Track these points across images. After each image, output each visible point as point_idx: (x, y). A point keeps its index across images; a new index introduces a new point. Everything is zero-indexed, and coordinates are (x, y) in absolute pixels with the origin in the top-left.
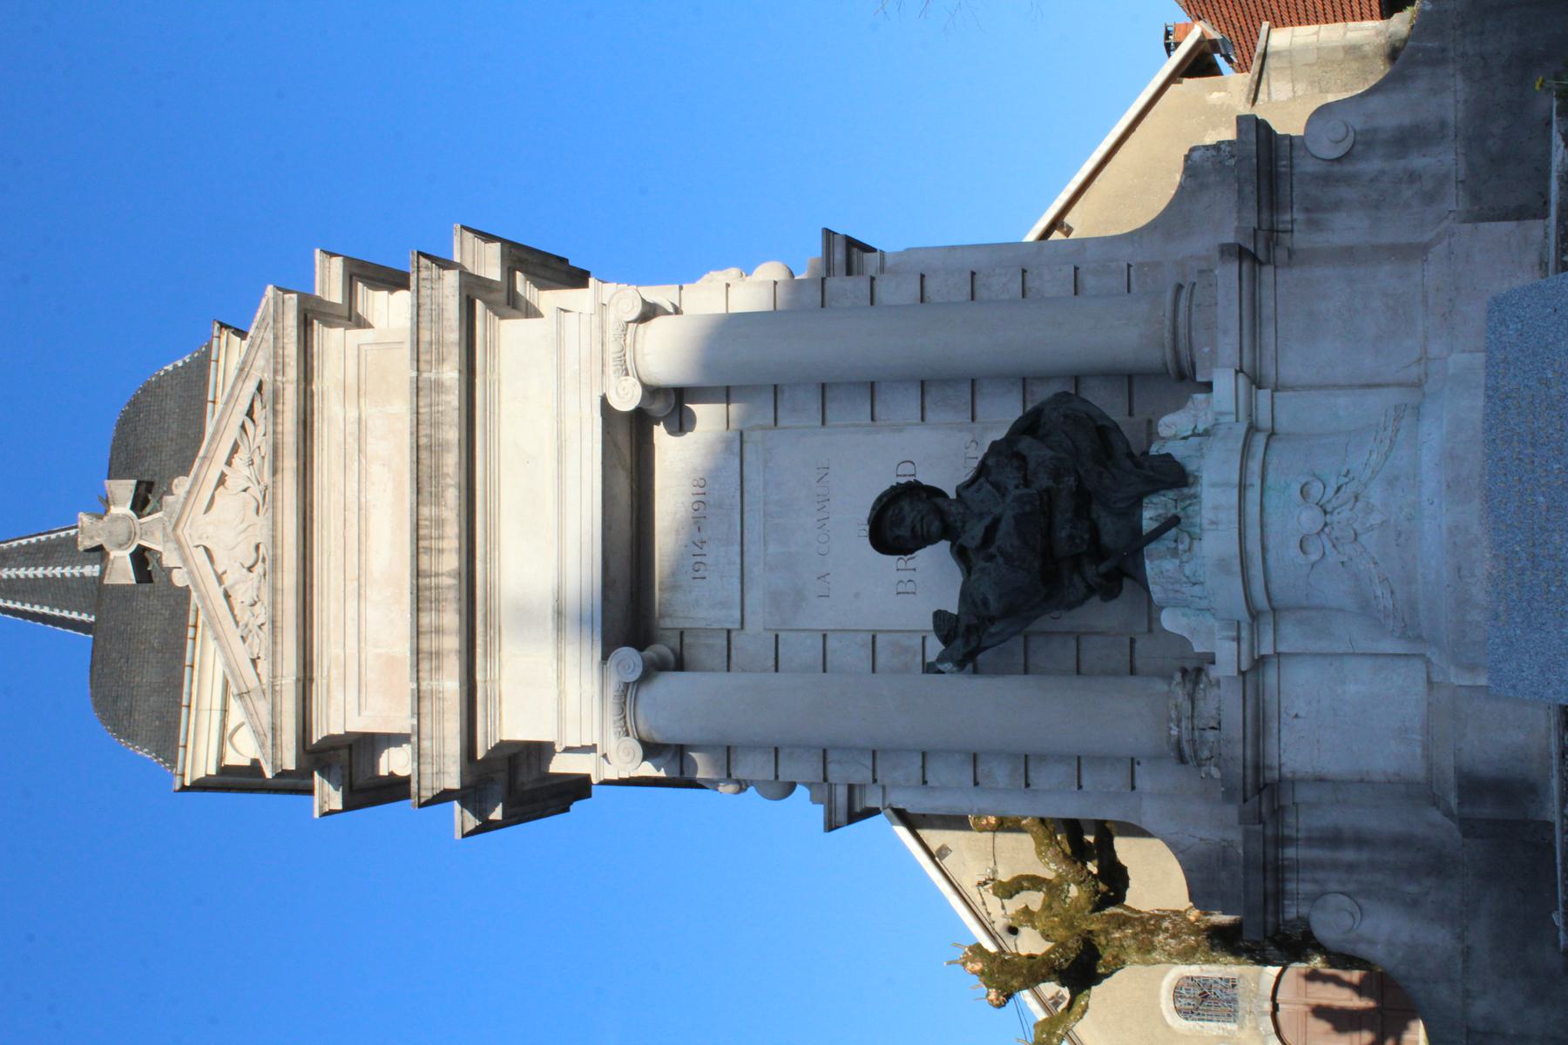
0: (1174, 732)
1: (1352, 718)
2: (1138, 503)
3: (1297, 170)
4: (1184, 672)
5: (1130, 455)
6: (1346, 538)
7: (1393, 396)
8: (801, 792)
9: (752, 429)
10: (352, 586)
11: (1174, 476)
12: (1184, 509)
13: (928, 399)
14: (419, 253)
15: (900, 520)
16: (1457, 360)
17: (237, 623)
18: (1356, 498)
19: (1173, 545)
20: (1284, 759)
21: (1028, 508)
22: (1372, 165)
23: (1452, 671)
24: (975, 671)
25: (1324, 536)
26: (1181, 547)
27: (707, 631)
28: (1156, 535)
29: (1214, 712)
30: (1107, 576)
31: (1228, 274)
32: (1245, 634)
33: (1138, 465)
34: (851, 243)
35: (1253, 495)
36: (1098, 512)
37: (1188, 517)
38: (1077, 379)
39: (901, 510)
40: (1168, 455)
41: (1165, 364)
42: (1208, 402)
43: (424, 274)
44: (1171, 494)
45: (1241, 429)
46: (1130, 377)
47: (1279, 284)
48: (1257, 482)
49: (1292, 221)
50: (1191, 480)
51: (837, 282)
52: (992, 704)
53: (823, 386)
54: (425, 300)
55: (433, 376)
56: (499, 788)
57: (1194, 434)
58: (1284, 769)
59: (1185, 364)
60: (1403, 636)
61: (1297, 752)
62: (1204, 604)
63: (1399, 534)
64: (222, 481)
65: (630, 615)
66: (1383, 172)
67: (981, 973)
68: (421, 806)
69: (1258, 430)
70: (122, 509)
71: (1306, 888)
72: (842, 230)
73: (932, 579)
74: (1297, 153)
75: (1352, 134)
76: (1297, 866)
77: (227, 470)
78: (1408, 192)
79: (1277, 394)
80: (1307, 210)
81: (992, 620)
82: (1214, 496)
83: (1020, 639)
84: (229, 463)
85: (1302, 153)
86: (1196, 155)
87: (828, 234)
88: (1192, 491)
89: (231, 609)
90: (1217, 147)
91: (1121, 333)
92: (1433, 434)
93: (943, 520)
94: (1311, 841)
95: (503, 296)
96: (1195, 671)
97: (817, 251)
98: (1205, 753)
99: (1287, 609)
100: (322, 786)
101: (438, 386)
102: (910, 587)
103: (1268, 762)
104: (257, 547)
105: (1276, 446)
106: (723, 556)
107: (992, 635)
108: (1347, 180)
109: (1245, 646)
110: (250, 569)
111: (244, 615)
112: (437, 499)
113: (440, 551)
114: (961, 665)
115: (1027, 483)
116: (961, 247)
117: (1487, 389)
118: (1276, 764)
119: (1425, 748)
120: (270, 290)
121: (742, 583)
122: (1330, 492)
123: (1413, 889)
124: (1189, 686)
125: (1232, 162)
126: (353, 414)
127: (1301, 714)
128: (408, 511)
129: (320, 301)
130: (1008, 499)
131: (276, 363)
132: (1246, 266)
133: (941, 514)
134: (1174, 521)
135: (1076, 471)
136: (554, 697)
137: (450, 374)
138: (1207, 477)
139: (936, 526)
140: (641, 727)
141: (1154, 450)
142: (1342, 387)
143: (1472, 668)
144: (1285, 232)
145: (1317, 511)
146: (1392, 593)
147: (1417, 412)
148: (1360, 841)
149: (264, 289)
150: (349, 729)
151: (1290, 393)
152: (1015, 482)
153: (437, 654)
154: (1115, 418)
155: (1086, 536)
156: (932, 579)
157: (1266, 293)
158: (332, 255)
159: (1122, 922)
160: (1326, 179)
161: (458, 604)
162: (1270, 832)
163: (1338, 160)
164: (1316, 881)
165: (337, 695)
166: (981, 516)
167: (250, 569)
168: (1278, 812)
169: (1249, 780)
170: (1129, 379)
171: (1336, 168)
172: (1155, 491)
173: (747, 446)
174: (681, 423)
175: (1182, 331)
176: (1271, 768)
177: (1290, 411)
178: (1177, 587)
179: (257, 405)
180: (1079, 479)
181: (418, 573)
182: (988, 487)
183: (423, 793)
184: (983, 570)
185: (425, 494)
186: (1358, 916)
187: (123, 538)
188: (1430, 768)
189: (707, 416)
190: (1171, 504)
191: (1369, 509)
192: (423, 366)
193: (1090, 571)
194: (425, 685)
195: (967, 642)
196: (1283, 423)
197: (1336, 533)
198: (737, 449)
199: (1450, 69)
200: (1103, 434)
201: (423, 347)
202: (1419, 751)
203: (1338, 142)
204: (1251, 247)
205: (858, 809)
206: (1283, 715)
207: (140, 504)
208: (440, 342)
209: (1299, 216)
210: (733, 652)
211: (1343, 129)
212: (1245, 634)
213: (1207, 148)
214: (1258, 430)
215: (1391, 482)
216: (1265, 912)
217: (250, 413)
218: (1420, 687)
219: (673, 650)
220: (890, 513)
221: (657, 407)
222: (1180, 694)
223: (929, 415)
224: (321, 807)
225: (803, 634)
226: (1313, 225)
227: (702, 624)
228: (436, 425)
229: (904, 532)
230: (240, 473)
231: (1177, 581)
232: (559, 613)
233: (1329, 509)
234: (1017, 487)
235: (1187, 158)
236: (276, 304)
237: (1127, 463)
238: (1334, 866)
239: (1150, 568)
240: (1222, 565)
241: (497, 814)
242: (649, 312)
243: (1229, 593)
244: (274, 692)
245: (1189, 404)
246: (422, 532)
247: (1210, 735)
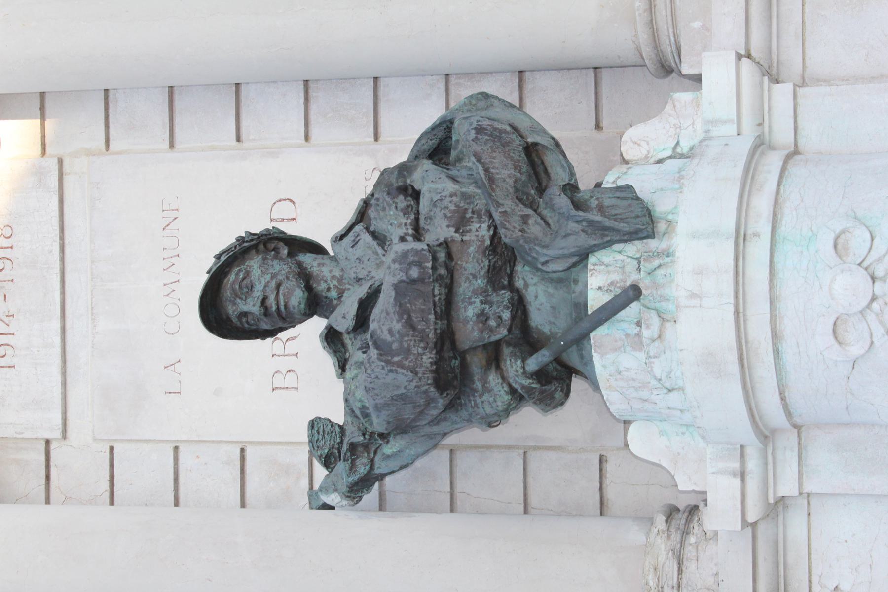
4: (671, 512)
5: (571, 188)
15: (243, 294)
19: (635, 330)
21: (415, 273)
26: (646, 333)
28: (609, 311)
30: (541, 375)
32: (753, 464)
33: (578, 205)
35: (758, 251)
36: (524, 276)
37: (656, 286)
39: (247, 274)
40: (629, 188)
42: (697, 104)
44: (633, 249)
45: (745, 145)
48: (765, 230)
50: (661, 227)
59: (668, 50)
62: (687, 418)
69: (772, 148)
73: (296, 380)
79: (801, 91)
93: (309, 288)
102: (291, 381)
105: (797, 170)
107: (388, 457)
115: (418, 234)
121: (64, 374)
124: (676, 537)
130: (392, 255)
134: (633, 293)
135: (491, 216)
139: (297, 298)
151: (823, 89)
152: (401, 232)
155: (506, 315)
156: (296, 380)
173: (68, 181)
177: (824, 118)
178: (645, 394)
182: (366, 238)
193: (513, 367)
195: (352, 468)
196: (813, 137)
200: (536, 160)
212: (753, 464)
220: (232, 277)
222: (662, 548)
229: (252, 306)
234: (402, 239)
237: (563, 202)
243: (725, 404)
245: (669, 108)
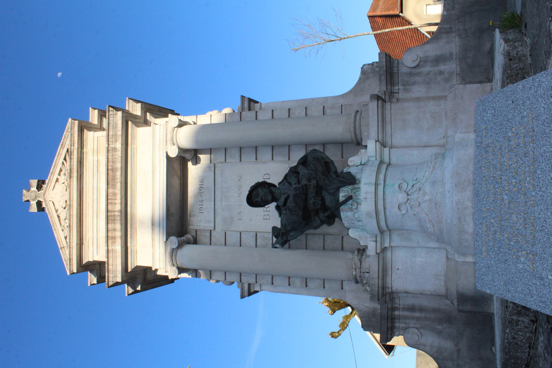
0: (354, 273)
1: (417, 270)
2: (338, 190)
3: (400, 71)
6: (421, 194)
7: (435, 150)
8: (236, 284)
9: (218, 163)
10: (95, 214)
11: (351, 180)
12: (354, 193)
13: (274, 152)
14: (109, 106)
15: (259, 195)
16: (459, 136)
17: (61, 225)
18: (420, 190)
19: (351, 206)
20: (393, 284)
21: (298, 192)
22: (427, 69)
23: (456, 256)
24: (289, 247)
25: (407, 204)
26: (353, 207)
27: (204, 230)
28: (344, 202)
29: (368, 267)
30: (328, 217)
31: (373, 105)
32: (379, 239)
33: (338, 176)
34: (250, 100)
35: (381, 188)
36: (324, 193)
37: (356, 196)
38: (324, 145)
39: (258, 192)
40: (350, 172)
41: (352, 139)
42: (366, 152)
43: (111, 113)
45: (377, 162)
46: (342, 144)
47: (392, 109)
48: (382, 183)
49: (399, 89)
50: (358, 182)
51: (246, 114)
52: (290, 259)
53: (241, 148)
54: (111, 122)
55: (113, 146)
56: (140, 280)
57: (361, 165)
58: (393, 288)
59: (359, 139)
60: (438, 241)
61: (398, 282)
62: (363, 228)
63: (436, 204)
64: (57, 180)
65: (178, 224)
66: (430, 71)
67: (327, 306)
68: (109, 287)
69: (384, 163)
70: (34, 189)
71: (402, 325)
72: (247, 95)
73: (268, 217)
74: (400, 66)
75: (419, 58)
76: (399, 318)
77: (59, 177)
78: (439, 78)
80: (404, 85)
81: (290, 231)
82: (366, 188)
83: (305, 236)
84: (59, 175)
85: (402, 66)
86: (365, 67)
87: (243, 97)
88: (358, 186)
89: (60, 221)
90: (372, 64)
91: (337, 128)
92: (449, 165)
94: (404, 309)
95: (142, 120)
96: (362, 251)
97: (239, 103)
98: (365, 282)
99: (394, 230)
100: (91, 276)
101: (115, 149)
102: (268, 217)
103: (387, 285)
104: (66, 201)
105: (390, 169)
106: (208, 205)
108: (418, 74)
109: (378, 244)
110: (65, 208)
111: (63, 223)
112: (114, 186)
113: (115, 204)
114: (283, 244)
116: (287, 101)
117: (476, 142)
118: (390, 286)
119: (445, 282)
122: (410, 187)
123: (440, 327)
124: (360, 256)
125: (378, 69)
126: (96, 159)
127: (400, 268)
128: (109, 190)
129: (91, 124)
131: (71, 143)
132: (380, 102)
133: (272, 193)
134: (350, 198)
136: (151, 251)
137: (119, 145)
138: (363, 181)
139: (270, 197)
140: (178, 263)
141: (345, 171)
142: (415, 147)
143: (464, 255)
144: (396, 93)
145: (405, 195)
146: (433, 226)
147: (443, 156)
148: (421, 309)
149: (68, 119)
150: (95, 259)
151: (396, 149)
152: (295, 182)
153: (114, 238)
154: (332, 159)
155: (320, 202)
156: (268, 217)
157: (388, 112)
158: (95, 109)
160: (410, 74)
161: (123, 220)
162: (390, 306)
163: (415, 67)
164: (405, 323)
165: (91, 248)
166: (284, 194)
167: (65, 208)
168: (392, 300)
169: (380, 292)
170: (341, 144)
171: (414, 70)
172: (344, 186)
173: (216, 169)
174: (196, 161)
175: (357, 127)
176: (389, 288)
177: (396, 156)
178: (353, 222)
179: (67, 156)
180: (317, 181)
181: (108, 211)
182: (286, 183)
183: (110, 283)
184: (284, 214)
185: (110, 185)
186: (420, 336)
187: (34, 198)
188: (447, 290)
189: (204, 158)
190: (350, 191)
191: (425, 194)
192: (110, 143)
193: (322, 215)
194: (110, 248)
195: (282, 238)
196: (394, 160)
197: (412, 203)
198: (213, 169)
199: (454, 35)
201: (110, 137)
202: (443, 283)
203: (414, 61)
204: (383, 97)
205: (252, 291)
206: (393, 269)
207: (39, 187)
208: (115, 135)
209: (401, 87)
210: (212, 238)
211: (416, 57)
212: (379, 239)
213: (369, 64)
214: (384, 163)
215: (434, 183)
216: (387, 334)
217: (65, 159)
218: (444, 259)
219: (193, 237)
221: (187, 156)
223: (274, 158)
224: (90, 283)
225: (234, 232)
226: (406, 90)
227: (202, 228)
228: (114, 162)
229: (259, 199)
230: (62, 179)
231: (353, 220)
232: (153, 224)
233: (409, 193)
234: (295, 184)
235: (362, 68)
236: (71, 124)
237: (334, 175)
238: (413, 318)
239: (342, 214)
240: (368, 214)
241: (139, 288)
242: (182, 124)
244: (70, 248)
245: (359, 153)
246: (109, 197)
247: (367, 275)
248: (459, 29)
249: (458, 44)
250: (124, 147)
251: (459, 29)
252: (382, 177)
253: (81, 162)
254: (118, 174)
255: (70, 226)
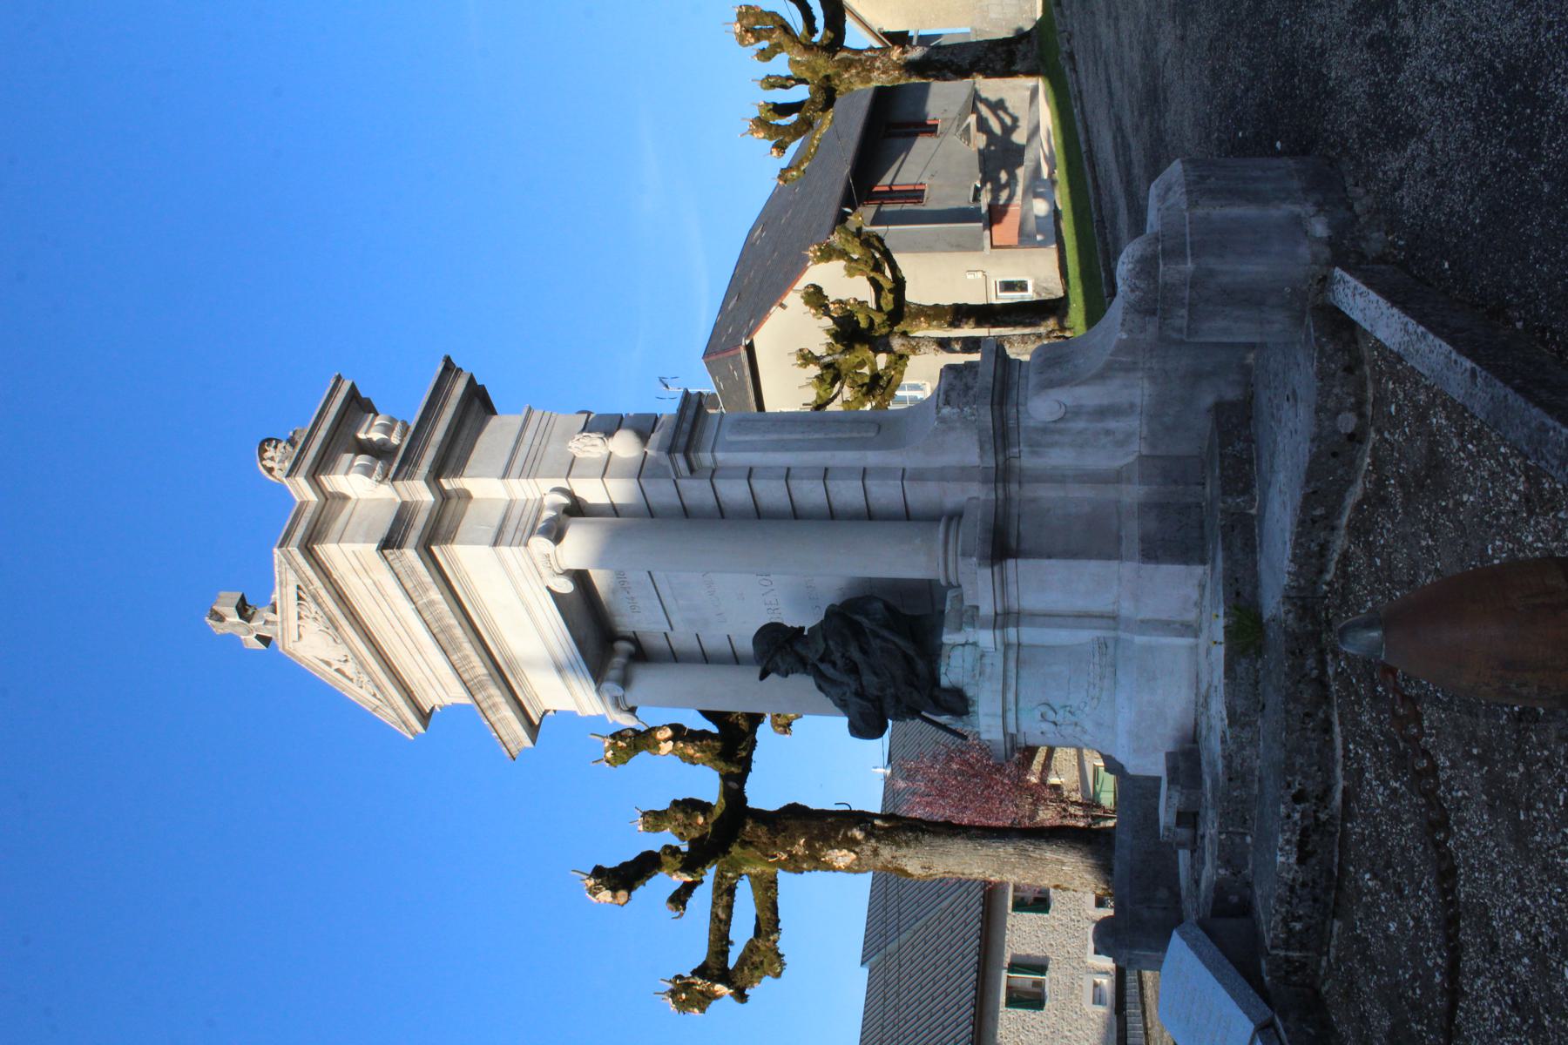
3: (1022, 425)
10: (414, 651)
22: (1080, 424)
108: (1060, 432)
112: (458, 648)
120: (276, 550)
126: (369, 582)
137: (435, 594)
159: (848, 64)
185: (450, 650)
199: (1140, 374)
208: (421, 583)
209: (1024, 449)
248: (1151, 369)
249: (1147, 392)
250: (447, 592)
251: (1151, 369)
252: (1011, 697)
253: (341, 598)
254: (458, 632)
255: (362, 664)
